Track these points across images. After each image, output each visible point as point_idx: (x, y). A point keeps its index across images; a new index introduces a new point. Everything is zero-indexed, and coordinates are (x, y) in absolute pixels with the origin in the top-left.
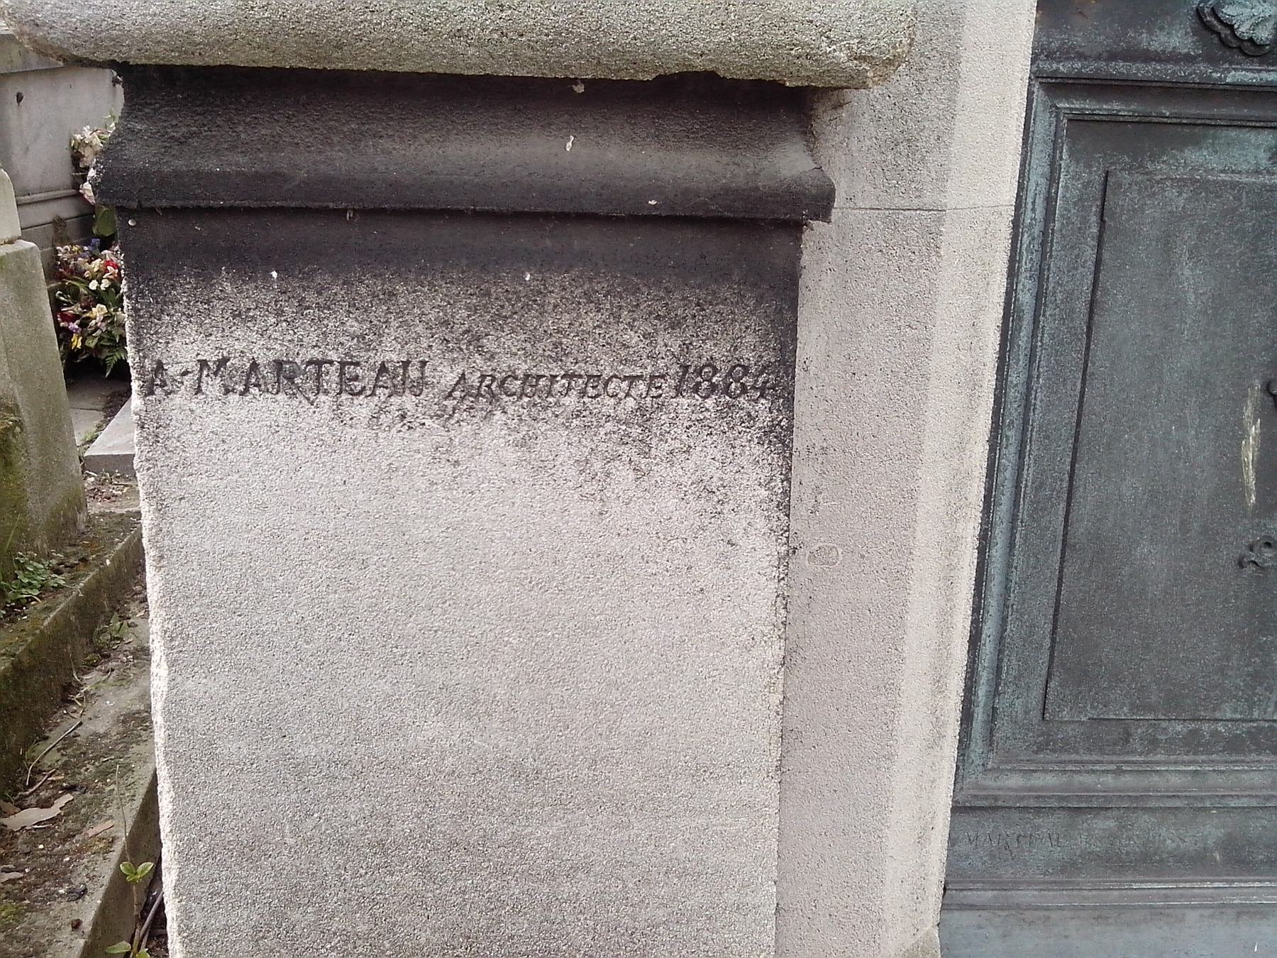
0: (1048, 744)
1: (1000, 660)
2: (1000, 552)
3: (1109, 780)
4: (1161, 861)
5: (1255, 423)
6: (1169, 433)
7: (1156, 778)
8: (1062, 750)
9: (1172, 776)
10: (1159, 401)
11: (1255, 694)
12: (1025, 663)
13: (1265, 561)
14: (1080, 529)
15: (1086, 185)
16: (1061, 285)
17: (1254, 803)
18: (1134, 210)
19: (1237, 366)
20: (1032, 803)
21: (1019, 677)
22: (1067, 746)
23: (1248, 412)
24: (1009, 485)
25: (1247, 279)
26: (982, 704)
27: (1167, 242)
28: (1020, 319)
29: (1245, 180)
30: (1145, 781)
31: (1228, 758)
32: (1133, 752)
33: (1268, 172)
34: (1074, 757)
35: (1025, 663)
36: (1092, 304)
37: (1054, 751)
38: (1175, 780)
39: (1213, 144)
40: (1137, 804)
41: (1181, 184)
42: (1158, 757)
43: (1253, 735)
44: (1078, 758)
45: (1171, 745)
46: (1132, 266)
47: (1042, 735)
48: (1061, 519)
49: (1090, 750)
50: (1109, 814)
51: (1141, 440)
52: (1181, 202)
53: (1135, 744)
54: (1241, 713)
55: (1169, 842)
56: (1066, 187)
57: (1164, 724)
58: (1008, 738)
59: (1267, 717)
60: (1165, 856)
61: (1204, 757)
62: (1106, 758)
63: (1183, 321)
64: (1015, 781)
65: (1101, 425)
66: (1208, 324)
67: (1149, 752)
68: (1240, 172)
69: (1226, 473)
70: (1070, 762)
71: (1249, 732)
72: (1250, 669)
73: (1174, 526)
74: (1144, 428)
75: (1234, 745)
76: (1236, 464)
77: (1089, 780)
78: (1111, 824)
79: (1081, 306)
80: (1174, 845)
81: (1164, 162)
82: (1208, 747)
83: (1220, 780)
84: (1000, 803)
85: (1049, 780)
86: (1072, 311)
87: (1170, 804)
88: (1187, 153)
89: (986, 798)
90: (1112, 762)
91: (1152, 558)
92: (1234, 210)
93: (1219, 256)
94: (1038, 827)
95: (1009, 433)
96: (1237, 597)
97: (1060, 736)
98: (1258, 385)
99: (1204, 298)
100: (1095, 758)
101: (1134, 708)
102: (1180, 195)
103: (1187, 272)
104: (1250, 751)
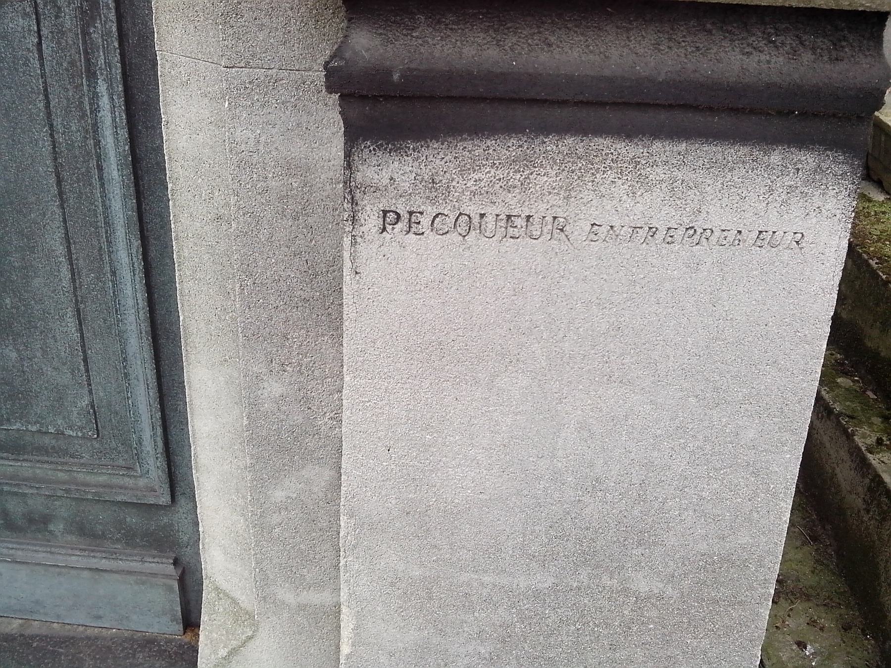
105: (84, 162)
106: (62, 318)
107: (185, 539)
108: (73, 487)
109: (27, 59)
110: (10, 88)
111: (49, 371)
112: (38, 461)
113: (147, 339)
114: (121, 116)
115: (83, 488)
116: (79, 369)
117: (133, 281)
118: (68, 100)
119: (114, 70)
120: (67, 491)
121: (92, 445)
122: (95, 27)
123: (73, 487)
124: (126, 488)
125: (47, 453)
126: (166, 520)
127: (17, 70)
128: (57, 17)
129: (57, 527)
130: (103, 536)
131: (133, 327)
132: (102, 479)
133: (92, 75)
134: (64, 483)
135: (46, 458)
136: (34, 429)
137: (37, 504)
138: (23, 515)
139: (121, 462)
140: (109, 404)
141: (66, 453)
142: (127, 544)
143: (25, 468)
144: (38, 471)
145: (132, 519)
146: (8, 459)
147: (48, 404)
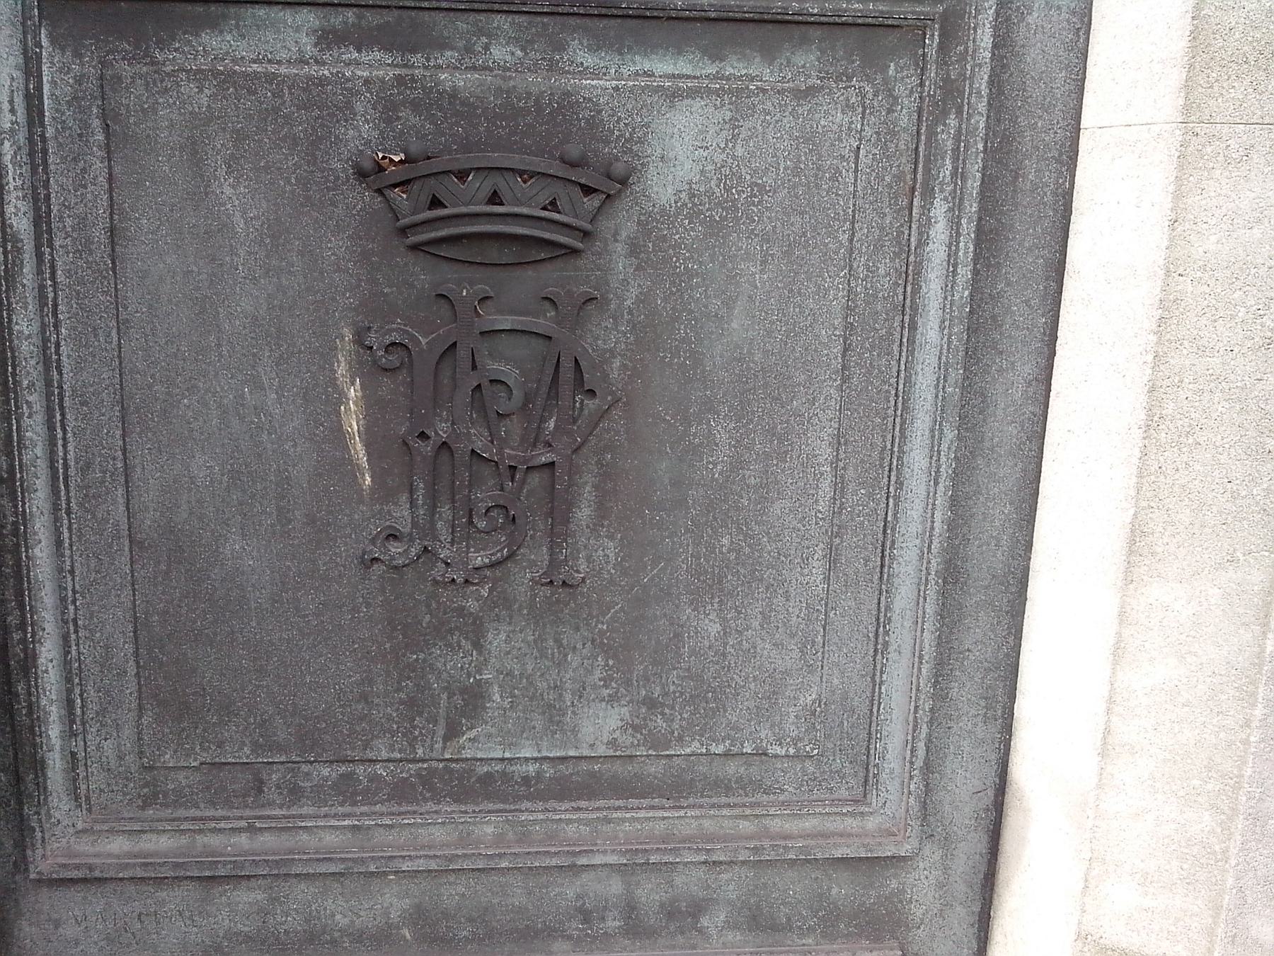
0: (155, 795)
1: (69, 691)
2: (46, 551)
3: (243, 840)
4: (333, 942)
5: (353, 384)
6: (242, 396)
7: (305, 837)
8: (176, 804)
9: (327, 834)
10: (221, 355)
11: (414, 727)
12: (108, 693)
13: (393, 558)
14: (148, 520)
15: (79, 80)
16: (68, 208)
17: (433, 865)
18: (143, 110)
19: (315, 310)
20: (140, 873)
21: (102, 712)
22: (180, 799)
23: (342, 370)
24: (42, 464)
25: (308, 198)
26: (57, 747)
27: (194, 152)
28: (19, 251)
29: (283, 70)
30: (286, 841)
31: (395, 809)
32: (271, 804)
33: (317, 62)
34: (193, 812)
35: (108, 693)
36: (112, 231)
37: (167, 806)
38: (330, 839)
39: (237, 26)
40: (279, 872)
41: (199, 76)
42: (305, 811)
43: (427, 779)
44: (198, 813)
45: (319, 794)
46: (153, 182)
47: (146, 785)
48: (122, 508)
49: (213, 804)
50: (253, 883)
51: (206, 405)
52: (205, 101)
53: (271, 794)
54: (400, 751)
55: (338, 917)
56: (53, 83)
57: (305, 768)
58: (101, 790)
59: (434, 755)
60: (337, 935)
61: (365, 809)
62: (237, 813)
63: (233, 252)
64: (119, 845)
65: (150, 387)
66: (267, 256)
67: (292, 803)
68: (279, 62)
69: (326, 447)
70: (186, 819)
71: (419, 775)
72: (403, 696)
73: (270, 514)
74: (207, 391)
75: (402, 792)
76: (338, 435)
77: (214, 841)
78: (260, 896)
79: (99, 234)
80: (346, 921)
81: (176, 50)
82: (369, 796)
83: (390, 837)
84: (97, 874)
85: (164, 843)
86: (89, 241)
87: (323, 868)
88: (205, 37)
89: (77, 867)
90: (242, 818)
91: (246, 555)
92: (276, 110)
93: (267, 168)
94: (163, 903)
95: (30, 399)
96: (368, 605)
97: (171, 786)
98: (349, 336)
99: (257, 224)
100: (220, 813)
101: (256, 747)
102: (201, 91)
103: (228, 191)
104: (425, 800)
105: (886, 320)
106: (805, 561)
107: (919, 913)
108: (767, 843)
109: (838, 171)
110: (802, 213)
111: (765, 648)
112: (713, 806)
113: (937, 583)
114: (967, 248)
115: (782, 843)
116: (813, 642)
117: (930, 497)
118: (882, 229)
119: (970, 182)
120: (756, 850)
121: (803, 770)
122: (945, 125)
123: (767, 843)
124: (850, 835)
125: (728, 790)
126: (894, 884)
127: (818, 186)
128: (890, 111)
129: (712, 921)
130: (788, 927)
131: (910, 569)
132: (809, 824)
133: (928, 194)
134: (750, 838)
135: (724, 800)
136: (720, 749)
137: (688, 882)
138: (662, 905)
139: (843, 793)
140: (845, 697)
141: (758, 786)
142: (824, 935)
143: (688, 820)
144: (706, 823)
145: (841, 889)
146: (663, 808)
147: (752, 704)
